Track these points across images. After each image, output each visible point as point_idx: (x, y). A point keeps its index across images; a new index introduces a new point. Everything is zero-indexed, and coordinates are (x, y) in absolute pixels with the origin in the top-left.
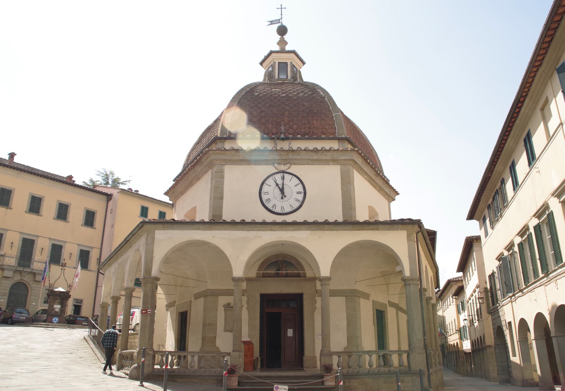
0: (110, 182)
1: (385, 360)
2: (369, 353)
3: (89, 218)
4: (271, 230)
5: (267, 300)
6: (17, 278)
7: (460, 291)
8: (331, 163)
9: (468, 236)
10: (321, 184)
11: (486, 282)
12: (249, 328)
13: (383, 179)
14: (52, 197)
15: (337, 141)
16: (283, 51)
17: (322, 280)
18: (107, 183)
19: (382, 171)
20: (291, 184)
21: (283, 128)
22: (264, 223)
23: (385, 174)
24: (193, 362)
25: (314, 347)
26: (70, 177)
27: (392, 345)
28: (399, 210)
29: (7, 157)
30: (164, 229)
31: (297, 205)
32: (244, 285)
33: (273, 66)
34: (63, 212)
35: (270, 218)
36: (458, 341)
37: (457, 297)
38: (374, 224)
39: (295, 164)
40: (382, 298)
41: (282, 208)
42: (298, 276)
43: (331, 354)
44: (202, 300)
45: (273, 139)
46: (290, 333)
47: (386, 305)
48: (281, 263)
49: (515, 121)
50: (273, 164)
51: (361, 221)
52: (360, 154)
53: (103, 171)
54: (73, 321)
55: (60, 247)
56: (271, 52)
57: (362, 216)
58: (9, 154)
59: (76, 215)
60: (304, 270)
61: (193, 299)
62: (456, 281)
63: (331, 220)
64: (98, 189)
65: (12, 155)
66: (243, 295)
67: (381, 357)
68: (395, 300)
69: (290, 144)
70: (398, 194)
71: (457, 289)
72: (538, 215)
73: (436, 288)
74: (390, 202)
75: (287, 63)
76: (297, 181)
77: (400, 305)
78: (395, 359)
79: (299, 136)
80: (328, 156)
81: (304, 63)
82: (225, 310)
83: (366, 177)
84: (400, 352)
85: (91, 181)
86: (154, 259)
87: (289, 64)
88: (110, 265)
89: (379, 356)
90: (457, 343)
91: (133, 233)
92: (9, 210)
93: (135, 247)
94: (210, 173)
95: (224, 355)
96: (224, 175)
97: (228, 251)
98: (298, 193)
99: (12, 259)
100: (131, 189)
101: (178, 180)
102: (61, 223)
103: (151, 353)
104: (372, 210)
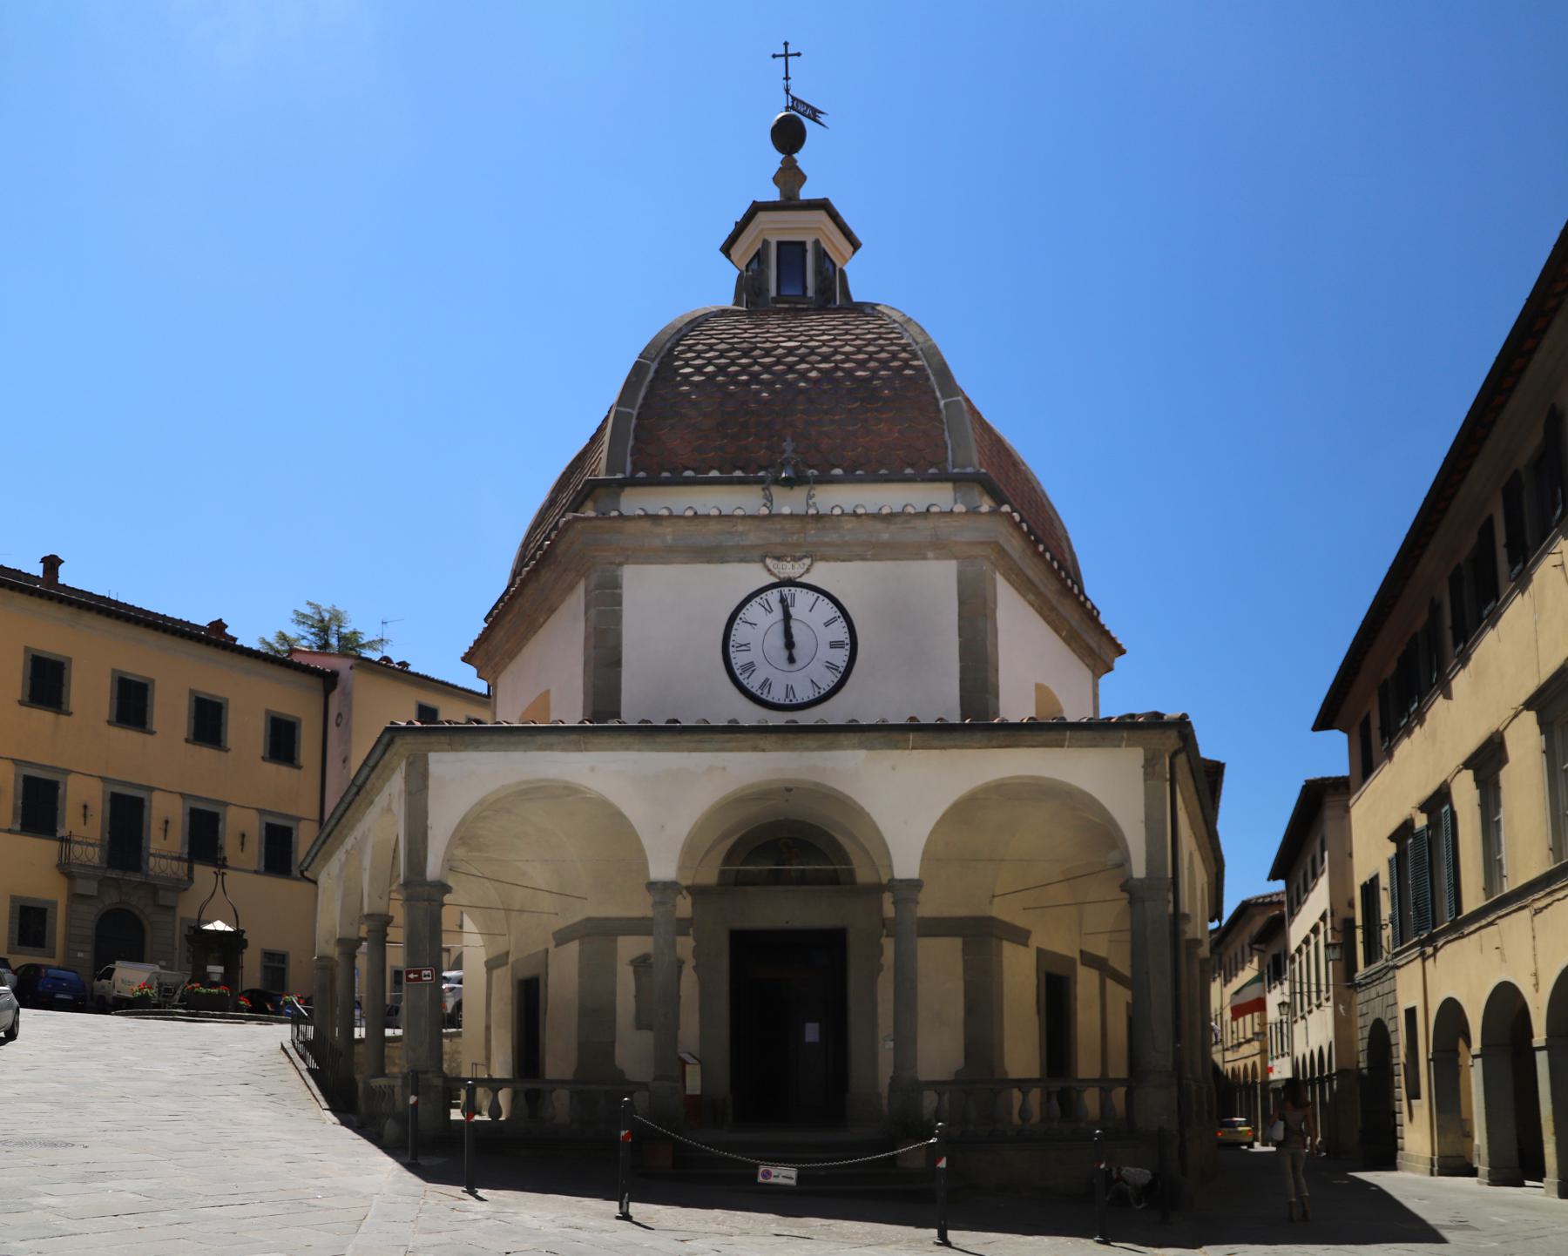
0: (334, 641)
1: (1066, 1101)
2: (1023, 1084)
3: (282, 741)
4: (755, 749)
5: (749, 950)
6: (112, 899)
7: (1276, 928)
8: (930, 554)
9: (1311, 777)
10: (887, 588)
11: (1351, 905)
12: (698, 1020)
13: (1083, 605)
14: (175, 682)
15: (949, 486)
16: (790, 202)
17: (895, 886)
18: (327, 645)
19: (1078, 580)
20: (810, 614)
21: (788, 446)
22: (733, 729)
23: (1088, 592)
24: (560, 1105)
25: (876, 1063)
26: (218, 626)
27: (1086, 1064)
28: (1121, 694)
29: (37, 570)
30: (452, 747)
31: (829, 680)
32: (684, 907)
33: (760, 257)
34: (208, 722)
35: (750, 714)
36: (1257, 1059)
37: (1262, 947)
38: (1048, 729)
39: (825, 559)
40: (1063, 944)
41: (790, 689)
42: (833, 880)
43: (920, 1087)
44: (573, 947)
45: (760, 481)
46: (812, 1032)
47: (1073, 960)
48: (788, 846)
49: (1503, 405)
50: (762, 560)
51: (1014, 718)
52: (1017, 526)
53: (308, 611)
54: (262, 1005)
55: (287, 832)
56: (756, 208)
57: (1015, 705)
58: (44, 560)
59: (246, 729)
60: (848, 861)
61: (553, 944)
62: (1263, 904)
63: (927, 718)
64: (296, 658)
65: (52, 563)
66: (684, 933)
67: (1054, 1100)
68: (1100, 949)
69: (810, 497)
70: (1121, 652)
71: (1263, 928)
72: (1424, 807)
73: (1212, 920)
74: (1097, 676)
75: (803, 244)
76: (832, 611)
77: (1111, 963)
78: (1091, 1101)
79: (838, 471)
80: (924, 529)
81: (856, 245)
82: (636, 972)
83: (1031, 597)
84: (1105, 1084)
85: (283, 637)
86: (430, 833)
87: (809, 247)
88: (329, 855)
89: (1049, 1093)
90: (1254, 1064)
91: (371, 763)
92: (63, 718)
93: (381, 801)
94: (580, 590)
95: (632, 1087)
96: (620, 596)
97: (635, 810)
98: (835, 645)
99: (90, 849)
100: (387, 659)
101: (496, 618)
102: (206, 753)
103: (438, 1082)
104: (1042, 692)
